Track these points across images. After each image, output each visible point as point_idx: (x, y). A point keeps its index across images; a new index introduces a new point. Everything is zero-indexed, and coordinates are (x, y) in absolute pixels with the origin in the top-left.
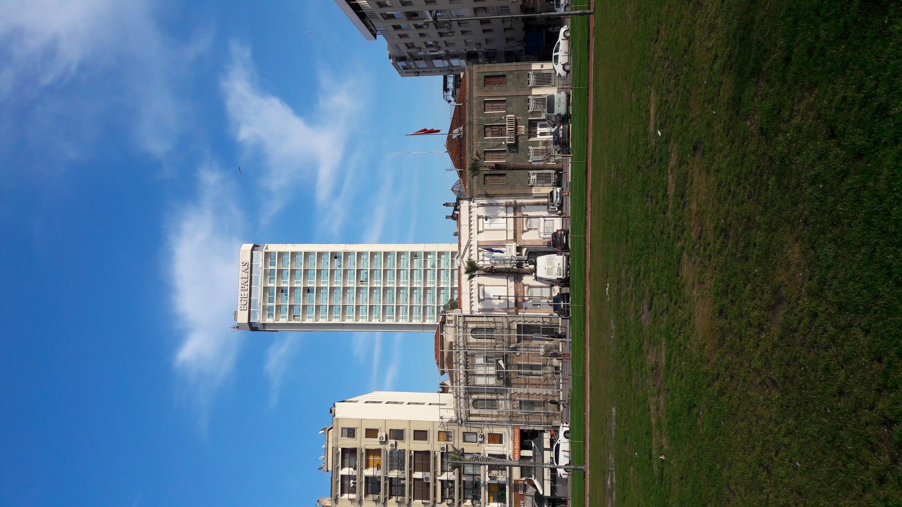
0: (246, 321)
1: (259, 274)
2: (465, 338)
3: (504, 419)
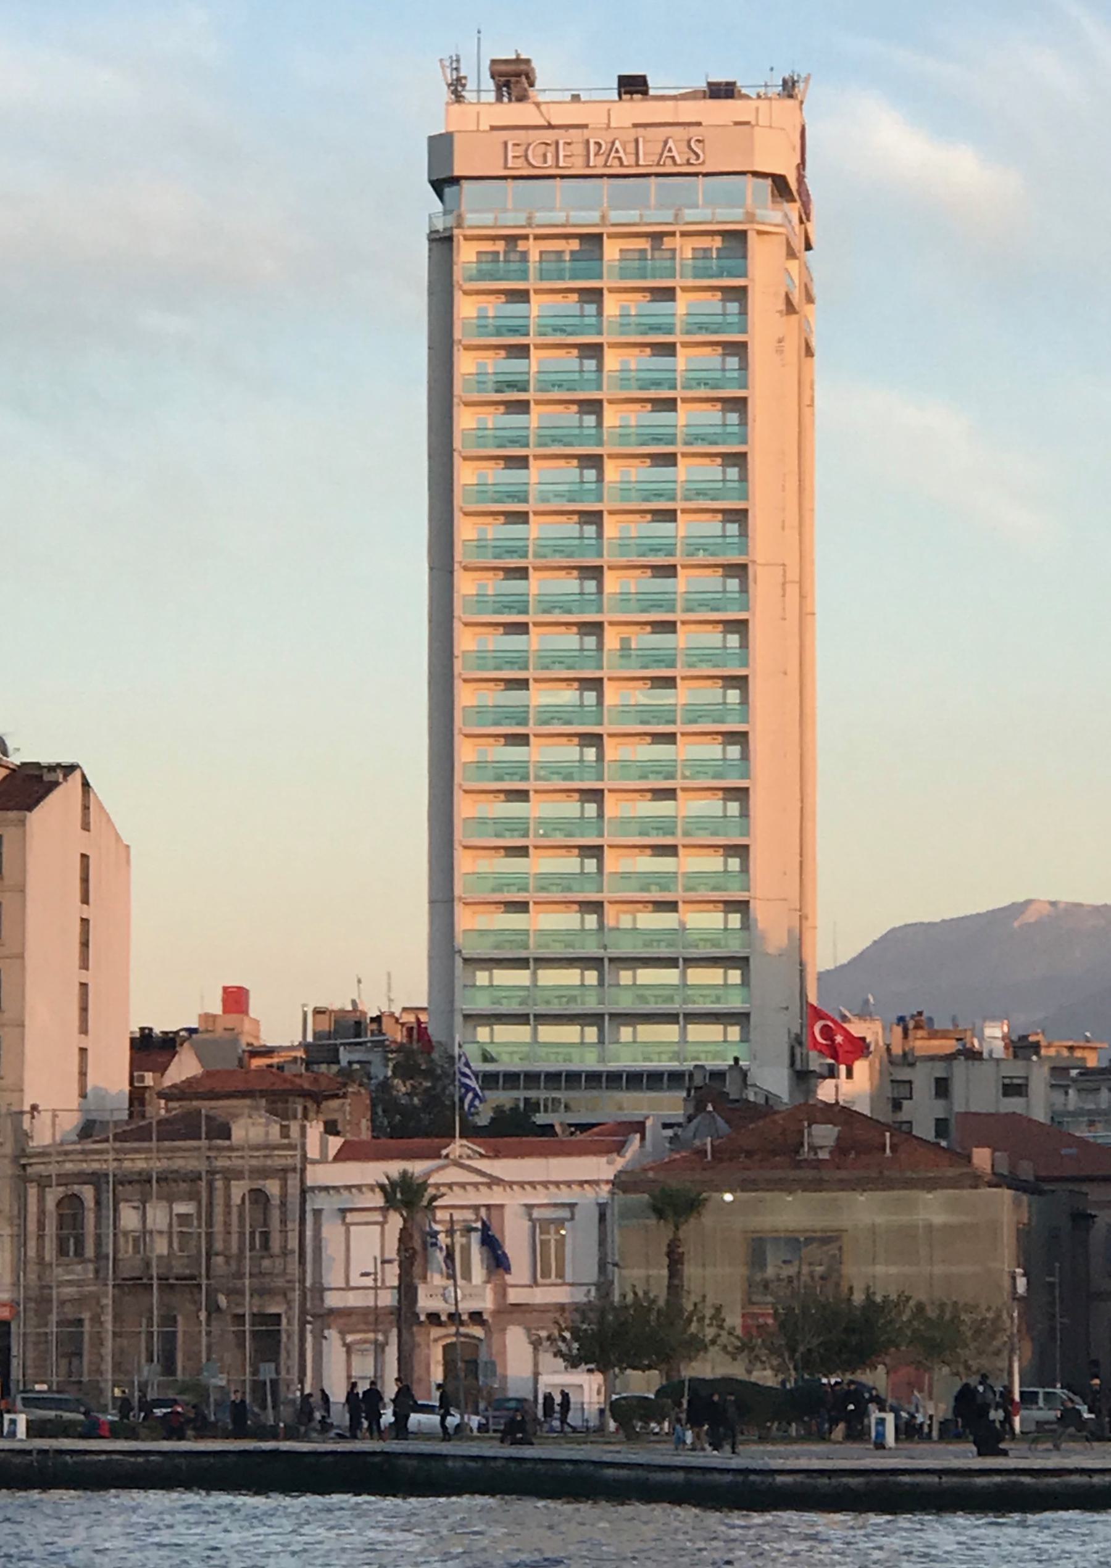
0: (457, 173)
1: (650, 206)
2: (239, 1175)
3: (33, 1277)
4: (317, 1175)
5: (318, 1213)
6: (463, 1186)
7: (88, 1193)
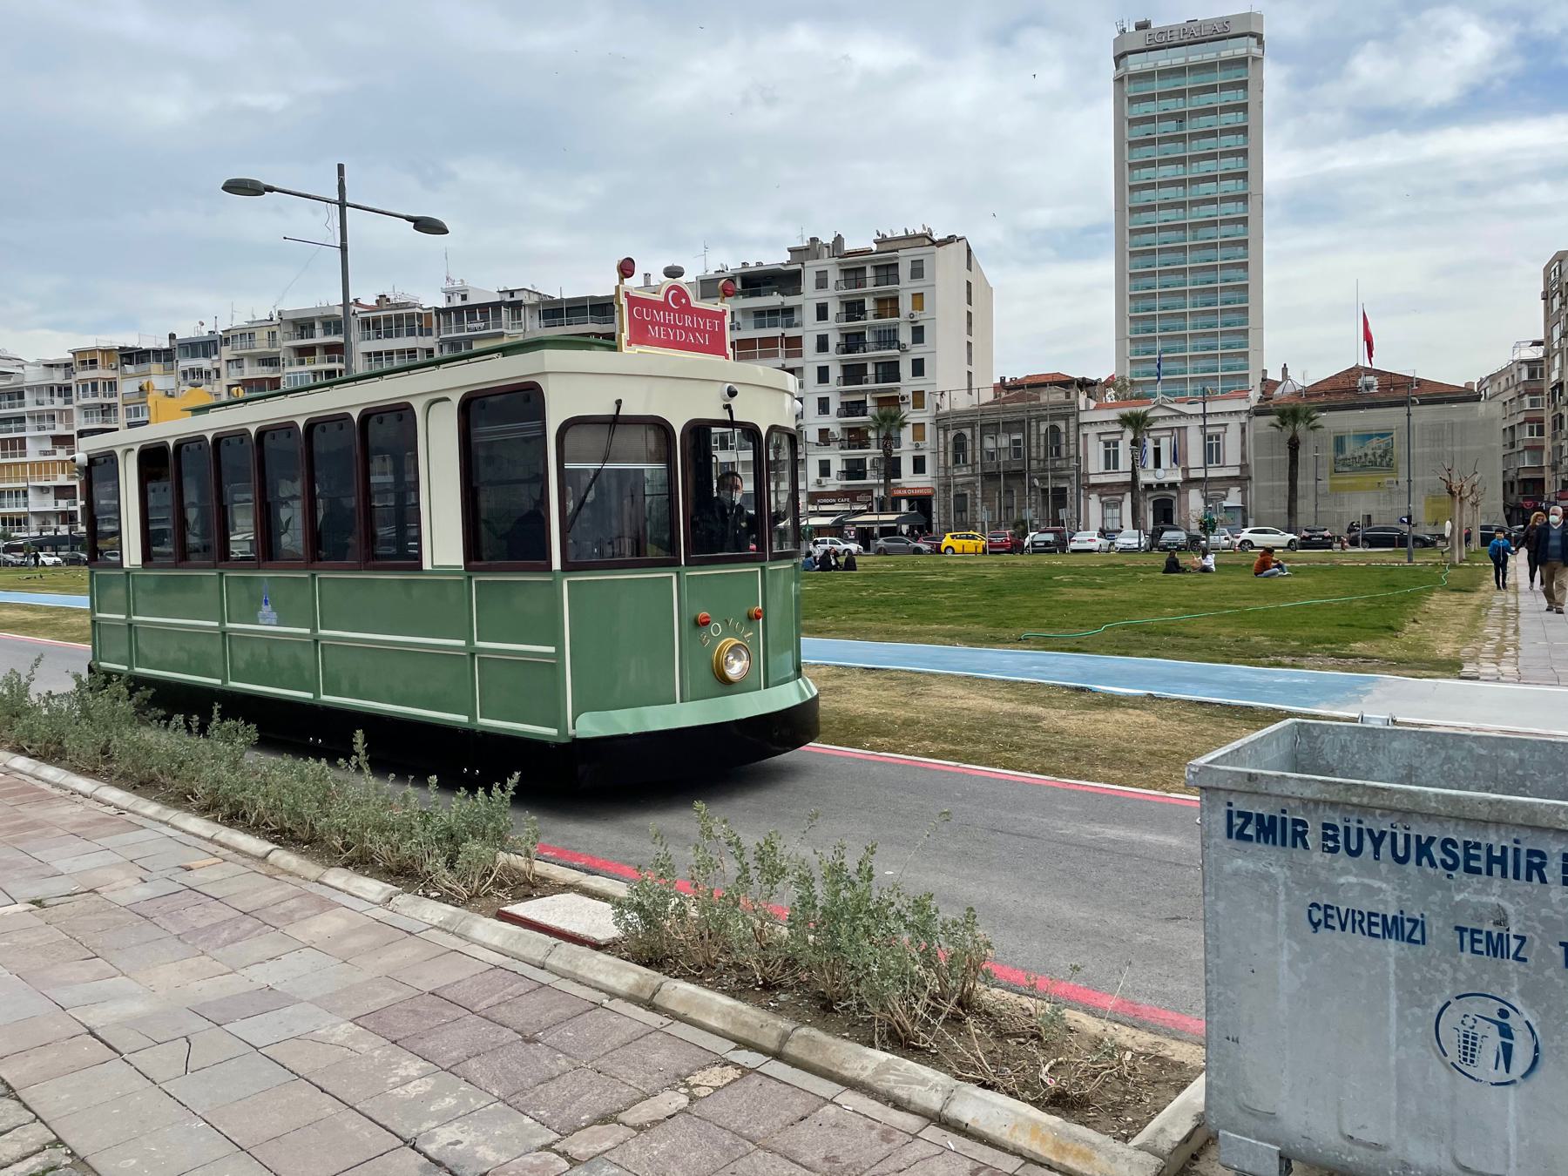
4: (1084, 418)
5: (1085, 435)
6: (1164, 418)
7: (967, 432)
